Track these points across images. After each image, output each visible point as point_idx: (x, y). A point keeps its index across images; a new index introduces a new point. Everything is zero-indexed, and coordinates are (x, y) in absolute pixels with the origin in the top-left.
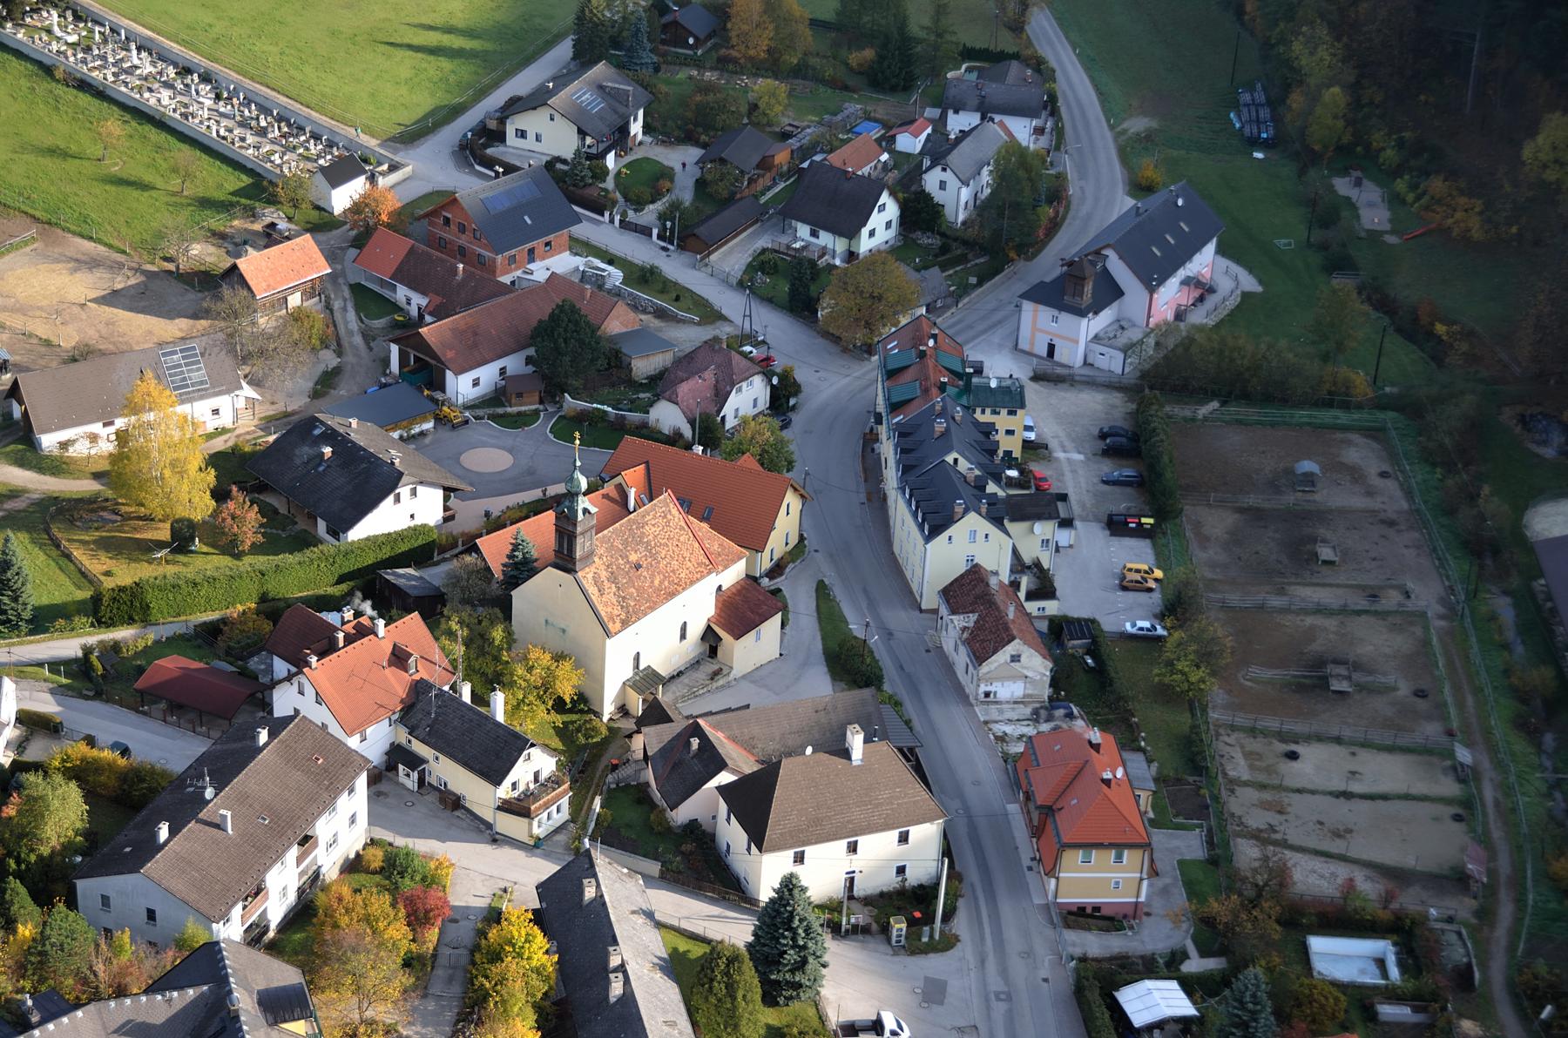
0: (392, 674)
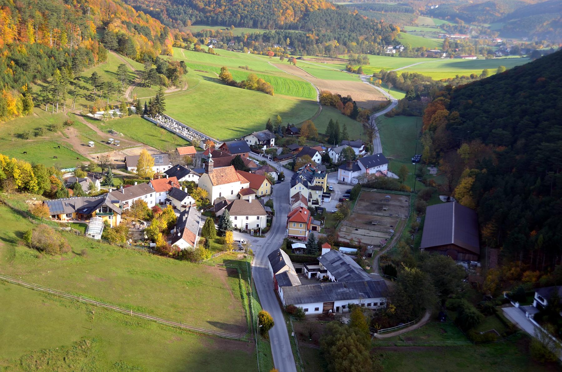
0: (168, 185)
